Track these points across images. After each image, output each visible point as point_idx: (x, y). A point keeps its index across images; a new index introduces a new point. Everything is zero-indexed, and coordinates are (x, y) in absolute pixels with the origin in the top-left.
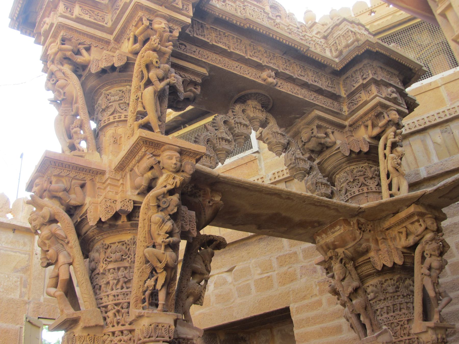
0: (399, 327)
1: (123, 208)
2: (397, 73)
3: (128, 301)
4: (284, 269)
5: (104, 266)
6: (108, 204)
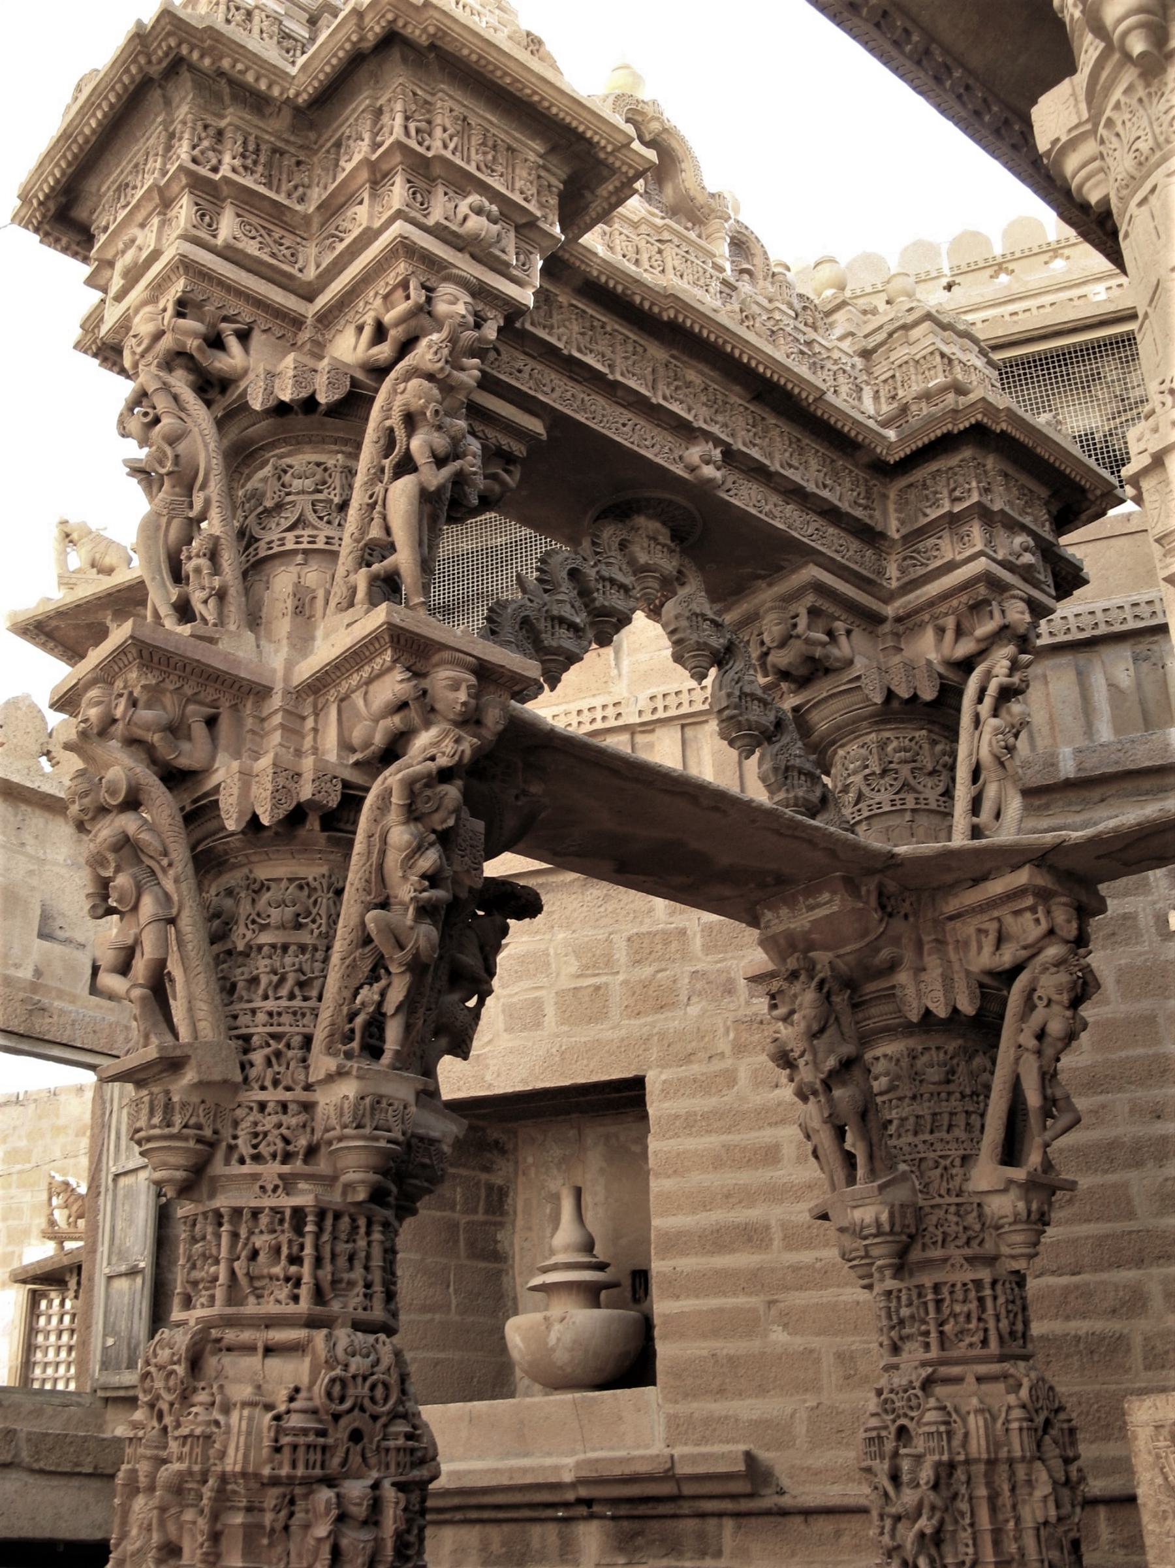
0: (938, 1171)
1: (317, 798)
2: (1044, 493)
3: (306, 1030)
4: (647, 971)
5: (249, 934)
6: (281, 781)
